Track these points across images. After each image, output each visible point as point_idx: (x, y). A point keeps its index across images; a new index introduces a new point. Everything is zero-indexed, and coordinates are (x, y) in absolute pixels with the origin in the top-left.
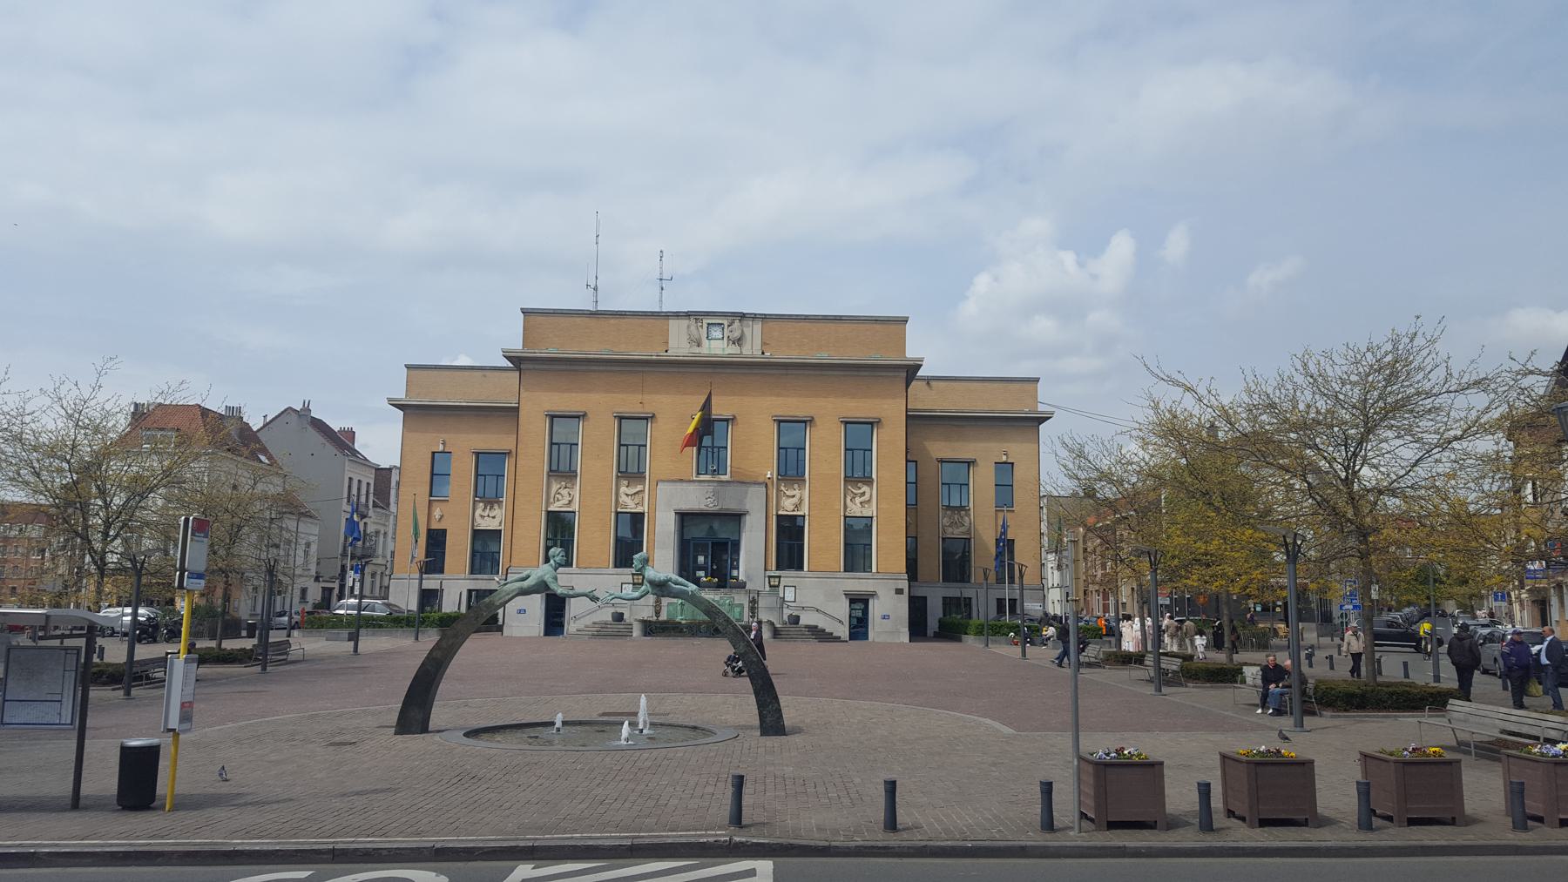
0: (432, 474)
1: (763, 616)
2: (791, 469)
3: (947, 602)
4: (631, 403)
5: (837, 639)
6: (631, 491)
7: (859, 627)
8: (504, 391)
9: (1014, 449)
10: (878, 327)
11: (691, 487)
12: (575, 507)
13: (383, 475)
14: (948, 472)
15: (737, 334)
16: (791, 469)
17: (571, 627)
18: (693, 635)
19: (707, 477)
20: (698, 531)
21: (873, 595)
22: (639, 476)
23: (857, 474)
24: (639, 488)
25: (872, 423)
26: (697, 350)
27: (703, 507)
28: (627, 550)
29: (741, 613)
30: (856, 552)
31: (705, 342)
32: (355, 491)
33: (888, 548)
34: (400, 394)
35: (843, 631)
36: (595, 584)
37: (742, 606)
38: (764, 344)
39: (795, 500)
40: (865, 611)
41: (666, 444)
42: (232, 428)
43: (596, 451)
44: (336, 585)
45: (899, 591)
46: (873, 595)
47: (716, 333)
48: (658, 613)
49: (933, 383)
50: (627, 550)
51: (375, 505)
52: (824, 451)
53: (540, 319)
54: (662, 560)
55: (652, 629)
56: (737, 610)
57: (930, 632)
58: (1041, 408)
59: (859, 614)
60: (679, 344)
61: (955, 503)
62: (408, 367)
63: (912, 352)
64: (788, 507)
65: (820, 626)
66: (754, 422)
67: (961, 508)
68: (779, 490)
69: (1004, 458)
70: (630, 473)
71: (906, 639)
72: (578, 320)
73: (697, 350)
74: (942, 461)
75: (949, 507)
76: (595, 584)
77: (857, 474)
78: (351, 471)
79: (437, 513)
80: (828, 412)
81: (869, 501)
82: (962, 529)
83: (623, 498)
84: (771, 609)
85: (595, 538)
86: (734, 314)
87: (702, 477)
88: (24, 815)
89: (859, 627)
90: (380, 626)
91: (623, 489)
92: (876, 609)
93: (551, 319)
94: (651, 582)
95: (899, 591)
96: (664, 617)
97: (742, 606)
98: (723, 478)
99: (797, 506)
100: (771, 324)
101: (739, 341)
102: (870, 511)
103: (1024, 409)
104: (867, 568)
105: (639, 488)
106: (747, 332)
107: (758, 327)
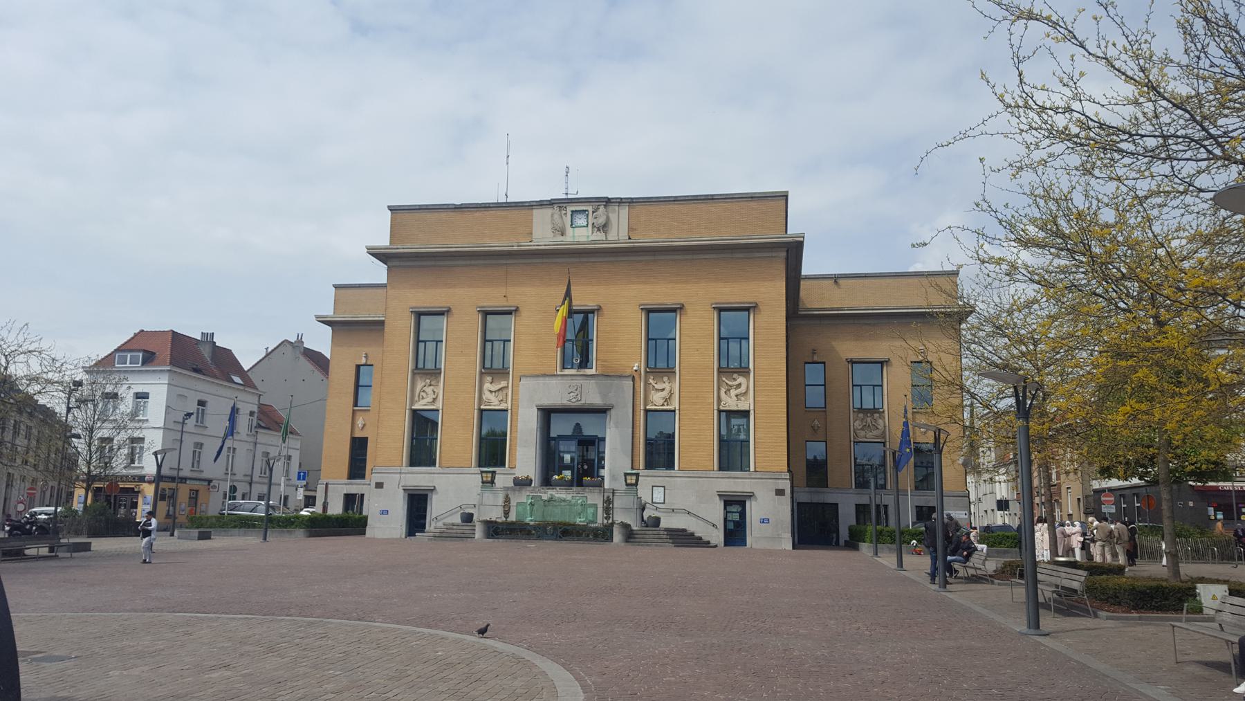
1: (619, 517)
2: (660, 360)
3: (862, 510)
4: (494, 297)
5: (707, 544)
6: (495, 387)
7: (735, 534)
10: (753, 204)
14: (859, 372)
15: (602, 220)
16: (660, 360)
17: (431, 526)
18: (539, 538)
19: (573, 372)
21: (751, 496)
22: (502, 372)
23: (731, 366)
24: (503, 384)
25: (747, 309)
26: (561, 238)
27: (565, 402)
28: (492, 451)
29: (595, 514)
30: (732, 453)
31: (569, 231)
33: (769, 444)
34: (328, 311)
35: (717, 536)
36: (456, 487)
37: (595, 506)
38: (630, 229)
39: (665, 394)
40: (743, 514)
42: (206, 352)
43: (459, 345)
45: (780, 492)
46: (751, 496)
47: (580, 220)
48: (506, 513)
49: (841, 281)
50: (492, 451)
52: (695, 339)
53: (407, 216)
54: (524, 458)
55: (494, 530)
56: (591, 511)
57: (842, 542)
59: (736, 517)
60: (542, 234)
61: (868, 404)
62: (337, 287)
64: (657, 400)
65: (691, 529)
66: (621, 307)
67: (875, 410)
70: (494, 369)
71: (789, 546)
72: (443, 215)
74: (852, 362)
75: (861, 410)
76: (456, 487)
77: (731, 366)
79: (360, 422)
80: (700, 296)
81: (746, 393)
82: (875, 433)
83: (487, 395)
84: (626, 510)
85: (457, 439)
87: (567, 372)
89: (735, 534)
90: (254, 526)
91: (487, 386)
92: (754, 511)
93: (417, 215)
95: (780, 492)
96: (512, 518)
97: (595, 506)
98: (588, 372)
99: (667, 400)
100: (638, 208)
101: (604, 228)
104: (744, 466)
105: (503, 384)
106: (613, 217)
107: (624, 211)
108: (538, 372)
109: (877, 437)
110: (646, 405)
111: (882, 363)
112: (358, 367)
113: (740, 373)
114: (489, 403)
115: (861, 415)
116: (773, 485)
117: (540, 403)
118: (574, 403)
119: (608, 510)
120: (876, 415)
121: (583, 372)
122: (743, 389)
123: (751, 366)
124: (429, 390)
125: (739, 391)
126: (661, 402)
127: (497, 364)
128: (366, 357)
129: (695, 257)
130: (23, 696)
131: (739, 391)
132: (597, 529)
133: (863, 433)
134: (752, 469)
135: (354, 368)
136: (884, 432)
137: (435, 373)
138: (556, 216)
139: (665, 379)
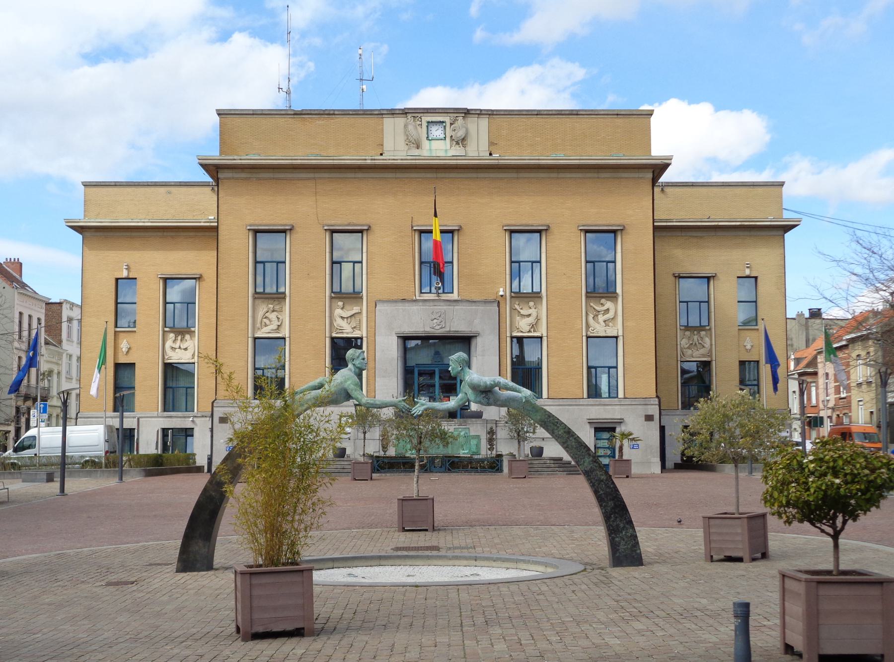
0: (117, 303)
6: (346, 314)
8: (201, 208)
9: (755, 257)
10: (619, 121)
11: (414, 308)
12: (285, 332)
13: (53, 309)
15: (461, 133)
20: (423, 358)
24: (356, 309)
25: (614, 232)
26: (416, 152)
27: (428, 329)
29: (478, 446)
31: (426, 144)
32: (25, 326)
34: (79, 216)
38: (491, 144)
39: (531, 320)
41: (384, 262)
43: (304, 265)
44: (12, 428)
45: (649, 418)
47: (437, 132)
48: (385, 448)
51: (47, 343)
53: (238, 120)
54: (386, 386)
56: (474, 442)
58: (786, 215)
60: (395, 147)
61: (694, 321)
63: (658, 149)
64: (523, 326)
68: (513, 309)
69: (747, 272)
73: (416, 152)
75: (687, 328)
78: (19, 305)
79: (124, 346)
82: (702, 351)
83: (339, 322)
86: (457, 111)
88: (270, 641)
91: (338, 312)
94: (475, 388)
95: (649, 418)
96: (392, 452)
97: (478, 437)
99: (534, 326)
100: (498, 120)
101: (462, 141)
102: (616, 329)
103: (767, 218)
105: (356, 309)
107: (484, 122)
108: (395, 297)
109: (704, 356)
110: (511, 332)
111: (708, 278)
112: (117, 279)
113: (608, 298)
114: (341, 331)
115: (688, 333)
116: (642, 411)
117: (398, 330)
118: (439, 331)
119: (491, 441)
120: (703, 333)
121: (444, 297)
122: (610, 315)
123: (619, 290)
124: (273, 316)
125: (607, 316)
126: (528, 328)
127: (347, 287)
128: (128, 269)
129: (561, 175)
130: (753, 659)
131: (607, 316)
132: (482, 460)
133: (690, 352)
134: (621, 395)
135: (114, 282)
136: (711, 350)
137: (279, 297)
138: (410, 127)
139: (531, 304)
